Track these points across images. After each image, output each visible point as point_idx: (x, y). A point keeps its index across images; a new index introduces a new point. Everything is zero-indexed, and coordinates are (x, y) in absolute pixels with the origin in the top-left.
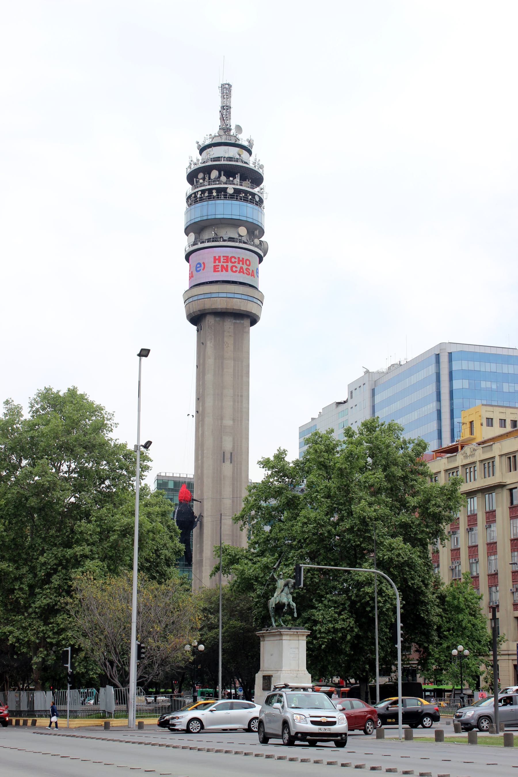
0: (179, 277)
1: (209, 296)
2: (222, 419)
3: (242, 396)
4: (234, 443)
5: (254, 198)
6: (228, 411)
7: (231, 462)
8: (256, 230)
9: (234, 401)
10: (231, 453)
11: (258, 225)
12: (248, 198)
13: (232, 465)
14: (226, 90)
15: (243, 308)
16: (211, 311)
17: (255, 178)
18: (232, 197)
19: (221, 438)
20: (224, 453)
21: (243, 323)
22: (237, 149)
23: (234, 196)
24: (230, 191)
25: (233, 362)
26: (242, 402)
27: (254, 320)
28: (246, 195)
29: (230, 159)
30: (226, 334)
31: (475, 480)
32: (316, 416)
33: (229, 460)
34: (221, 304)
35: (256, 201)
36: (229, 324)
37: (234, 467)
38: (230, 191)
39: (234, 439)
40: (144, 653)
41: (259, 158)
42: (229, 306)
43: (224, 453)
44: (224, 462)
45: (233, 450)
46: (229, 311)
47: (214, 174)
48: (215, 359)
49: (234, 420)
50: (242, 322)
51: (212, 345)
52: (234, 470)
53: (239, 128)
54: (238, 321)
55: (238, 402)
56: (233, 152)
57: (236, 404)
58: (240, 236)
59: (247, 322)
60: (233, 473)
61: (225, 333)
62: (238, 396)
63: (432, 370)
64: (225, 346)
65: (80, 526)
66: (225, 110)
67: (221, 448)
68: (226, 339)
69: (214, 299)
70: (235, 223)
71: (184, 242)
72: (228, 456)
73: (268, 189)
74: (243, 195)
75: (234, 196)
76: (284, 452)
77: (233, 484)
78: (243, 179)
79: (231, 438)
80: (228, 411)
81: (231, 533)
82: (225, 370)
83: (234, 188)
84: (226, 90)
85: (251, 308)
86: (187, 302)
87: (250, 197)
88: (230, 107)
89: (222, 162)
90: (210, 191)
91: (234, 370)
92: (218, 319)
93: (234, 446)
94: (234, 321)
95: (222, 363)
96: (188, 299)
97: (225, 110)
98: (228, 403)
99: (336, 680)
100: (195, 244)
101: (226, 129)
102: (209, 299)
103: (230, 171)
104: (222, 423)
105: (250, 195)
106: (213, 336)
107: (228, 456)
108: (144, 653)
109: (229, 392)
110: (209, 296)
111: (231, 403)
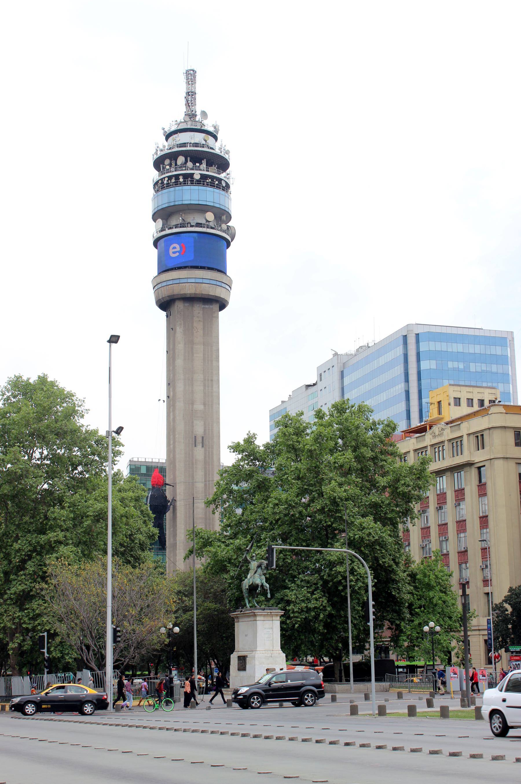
2: (193, 404)
3: (212, 380)
4: (205, 427)
5: (221, 183)
6: (199, 396)
7: (203, 446)
8: (223, 215)
9: (205, 386)
10: (203, 438)
11: (225, 210)
12: (214, 184)
13: (203, 449)
14: (191, 76)
15: (211, 293)
16: (179, 297)
17: (222, 164)
19: (193, 422)
20: (195, 437)
24: (197, 177)
26: (212, 386)
27: (222, 305)
29: (196, 145)
30: (195, 319)
31: (443, 459)
32: (286, 399)
33: (201, 445)
34: (189, 290)
35: (223, 187)
36: (198, 309)
37: (205, 450)
38: (197, 177)
39: (205, 424)
40: (119, 637)
43: (195, 437)
44: (195, 446)
45: (205, 434)
46: (198, 296)
47: (181, 160)
48: (185, 344)
49: (205, 404)
50: (211, 307)
52: (205, 454)
53: (204, 114)
54: (207, 306)
55: (208, 387)
56: (198, 138)
57: (207, 388)
58: (207, 221)
59: (216, 306)
60: (205, 457)
61: (194, 318)
62: (208, 380)
63: (399, 351)
66: (191, 96)
67: (193, 432)
68: (195, 324)
70: (202, 209)
72: (199, 440)
74: (210, 180)
77: (205, 468)
79: (202, 423)
80: (199, 396)
82: (195, 355)
84: (191, 76)
85: (219, 292)
87: (217, 182)
89: (189, 148)
90: (177, 177)
91: (204, 354)
92: (187, 305)
94: (203, 306)
95: (192, 348)
97: (191, 96)
98: (199, 388)
101: (191, 115)
102: (177, 285)
103: (195, 157)
104: (193, 408)
105: (216, 180)
106: (182, 322)
107: (199, 440)
108: (119, 637)
109: (199, 377)
111: (202, 388)
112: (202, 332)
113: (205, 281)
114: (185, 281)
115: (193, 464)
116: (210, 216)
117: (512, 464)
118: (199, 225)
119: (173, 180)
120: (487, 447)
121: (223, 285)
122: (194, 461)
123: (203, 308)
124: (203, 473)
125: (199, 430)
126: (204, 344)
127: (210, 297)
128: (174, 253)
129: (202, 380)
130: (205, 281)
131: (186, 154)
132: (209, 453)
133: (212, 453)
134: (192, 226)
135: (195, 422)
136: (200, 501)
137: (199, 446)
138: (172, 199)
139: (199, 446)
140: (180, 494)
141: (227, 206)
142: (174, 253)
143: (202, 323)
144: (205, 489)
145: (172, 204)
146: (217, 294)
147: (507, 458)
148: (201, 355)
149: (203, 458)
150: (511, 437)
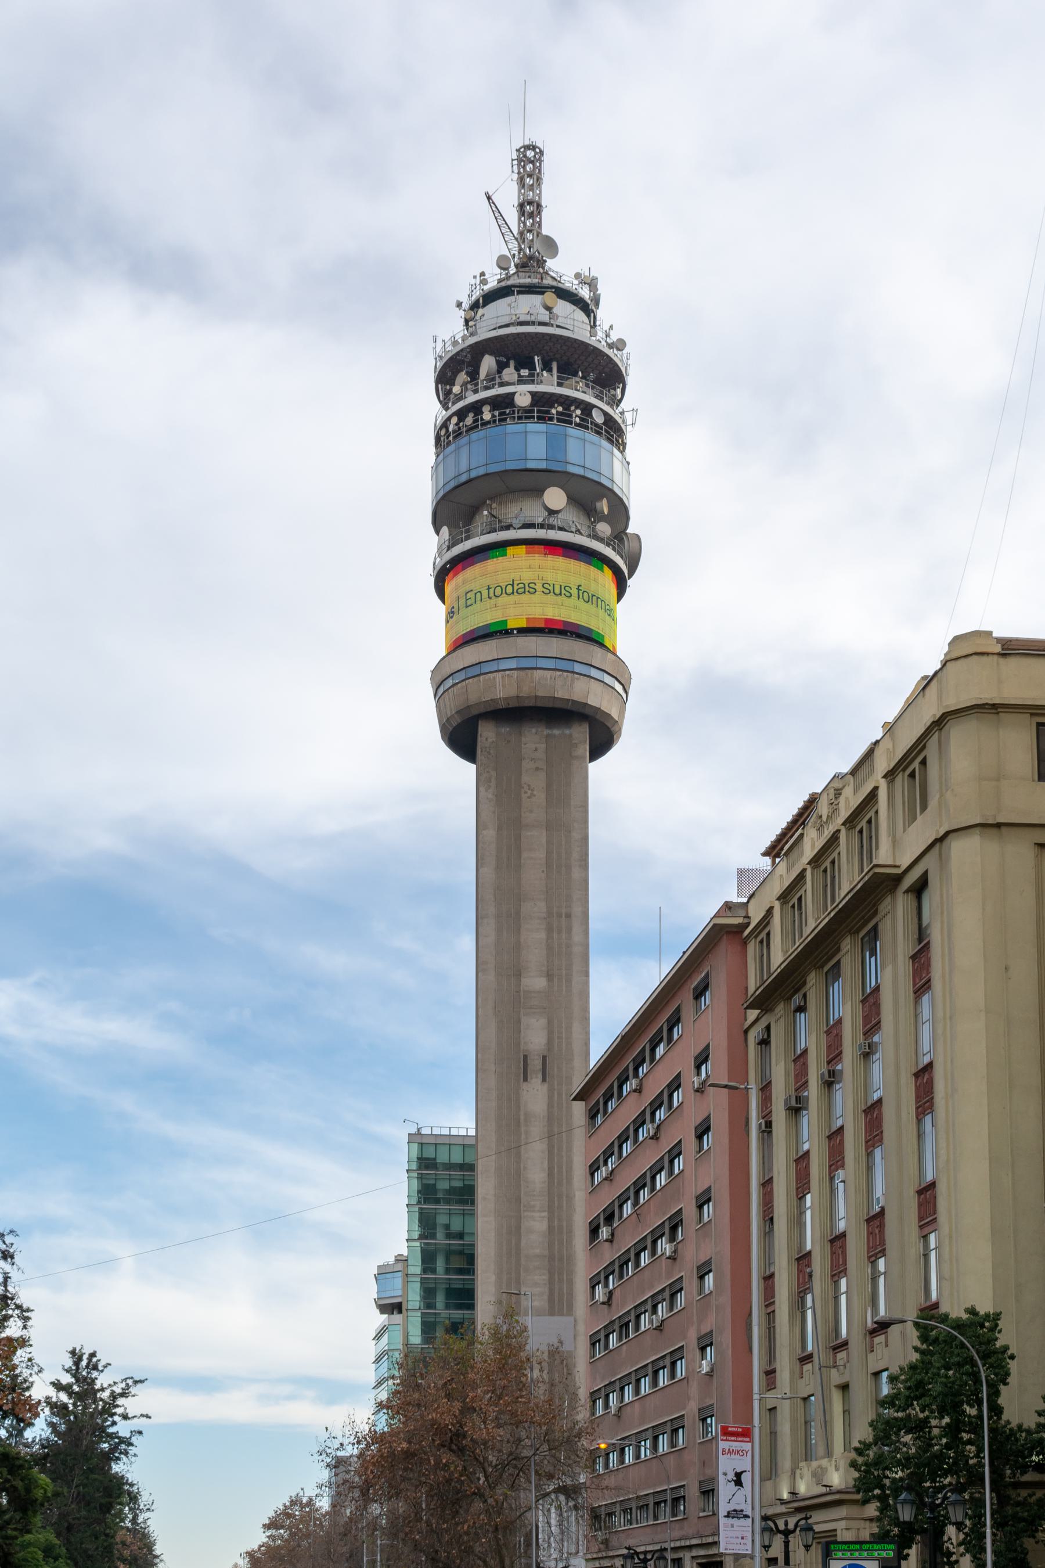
0: (425, 631)
1: (528, 666)
2: (518, 975)
3: (569, 916)
5: (590, 415)
6: (534, 955)
7: (544, 1080)
8: (601, 498)
9: (549, 930)
10: (544, 1058)
11: (600, 484)
12: (570, 416)
13: (546, 1086)
14: (529, 163)
15: (560, 694)
16: (483, 710)
17: (608, 376)
18: (526, 415)
19: (519, 1021)
20: (525, 1057)
21: (571, 735)
24: (523, 400)
25: (545, 834)
26: (569, 930)
28: (567, 408)
30: (526, 765)
33: (540, 1076)
35: (597, 425)
36: (533, 739)
37: (551, 1091)
38: (523, 400)
39: (550, 1022)
41: (616, 320)
43: (525, 1057)
44: (525, 1079)
45: (549, 1050)
47: (488, 363)
48: (500, 828)
49: (549, 976)
50: (567, 732)
51: (490, 796)
52: (550, 1098)
54: (556, 732)
55: (559, 932)
57: (555, 935)
58: (552, 513)
59: (580, 733)
60: (550, 1105)
61: (524, 763)
62: (560, 915)
64: (524, 796)
66: (530, 209)
68: (525, 778)
69: (486, 677)
71: (427, 547)
72: (536, 1064)
73: (637, 401)
74: (560, 409)
76: (264, 1526)
78: (567, 371)
79: (543, 1021)
80: (534, 955)
81: (546, 1253)
82: (525, 855)
84: (529, 163)
85: (595, 697)
86: (441, 691)
87: (578, 412)
88: (539, 206)
90: (476, 408)
91: (549, 853)
92: (505, 730)
94: (546, 732)
95: (518, 838)
96: (442, 681)
98: (534, 936)
100: (453, 543)
102: (475, 679)
103: (519, 351)
104: (518, 985)
106: (493, 773)
107: (536, 1064)
109: (535, 909)
110: (476, 671)
111: (543, 935)
112: (543, 796)
113: (542, 663)
114: (494, 666)
116: (555, 497)
117: (1020, 853)
119: (469, 420)
120: (933, 802)
121: (594, 673)
122: (522, 1118)
123: (547, 736)
125: (535, 1036)
126: (549, 827)
127: (558, 705)
129: (544, 915)
130: (542, 663)
135: (524, 1020)
136: (537, 1214)
137: (536, 1081)
138: (464, 467)
139: (536, 1081)
140: (484, 1199)
141: (604, 470)
143: (542, 775)
145: (464, 478)
146: (592, 701)
147: (999, 825)
148: (541, 854)
149: (546, 1108)
150: (1018, 746)
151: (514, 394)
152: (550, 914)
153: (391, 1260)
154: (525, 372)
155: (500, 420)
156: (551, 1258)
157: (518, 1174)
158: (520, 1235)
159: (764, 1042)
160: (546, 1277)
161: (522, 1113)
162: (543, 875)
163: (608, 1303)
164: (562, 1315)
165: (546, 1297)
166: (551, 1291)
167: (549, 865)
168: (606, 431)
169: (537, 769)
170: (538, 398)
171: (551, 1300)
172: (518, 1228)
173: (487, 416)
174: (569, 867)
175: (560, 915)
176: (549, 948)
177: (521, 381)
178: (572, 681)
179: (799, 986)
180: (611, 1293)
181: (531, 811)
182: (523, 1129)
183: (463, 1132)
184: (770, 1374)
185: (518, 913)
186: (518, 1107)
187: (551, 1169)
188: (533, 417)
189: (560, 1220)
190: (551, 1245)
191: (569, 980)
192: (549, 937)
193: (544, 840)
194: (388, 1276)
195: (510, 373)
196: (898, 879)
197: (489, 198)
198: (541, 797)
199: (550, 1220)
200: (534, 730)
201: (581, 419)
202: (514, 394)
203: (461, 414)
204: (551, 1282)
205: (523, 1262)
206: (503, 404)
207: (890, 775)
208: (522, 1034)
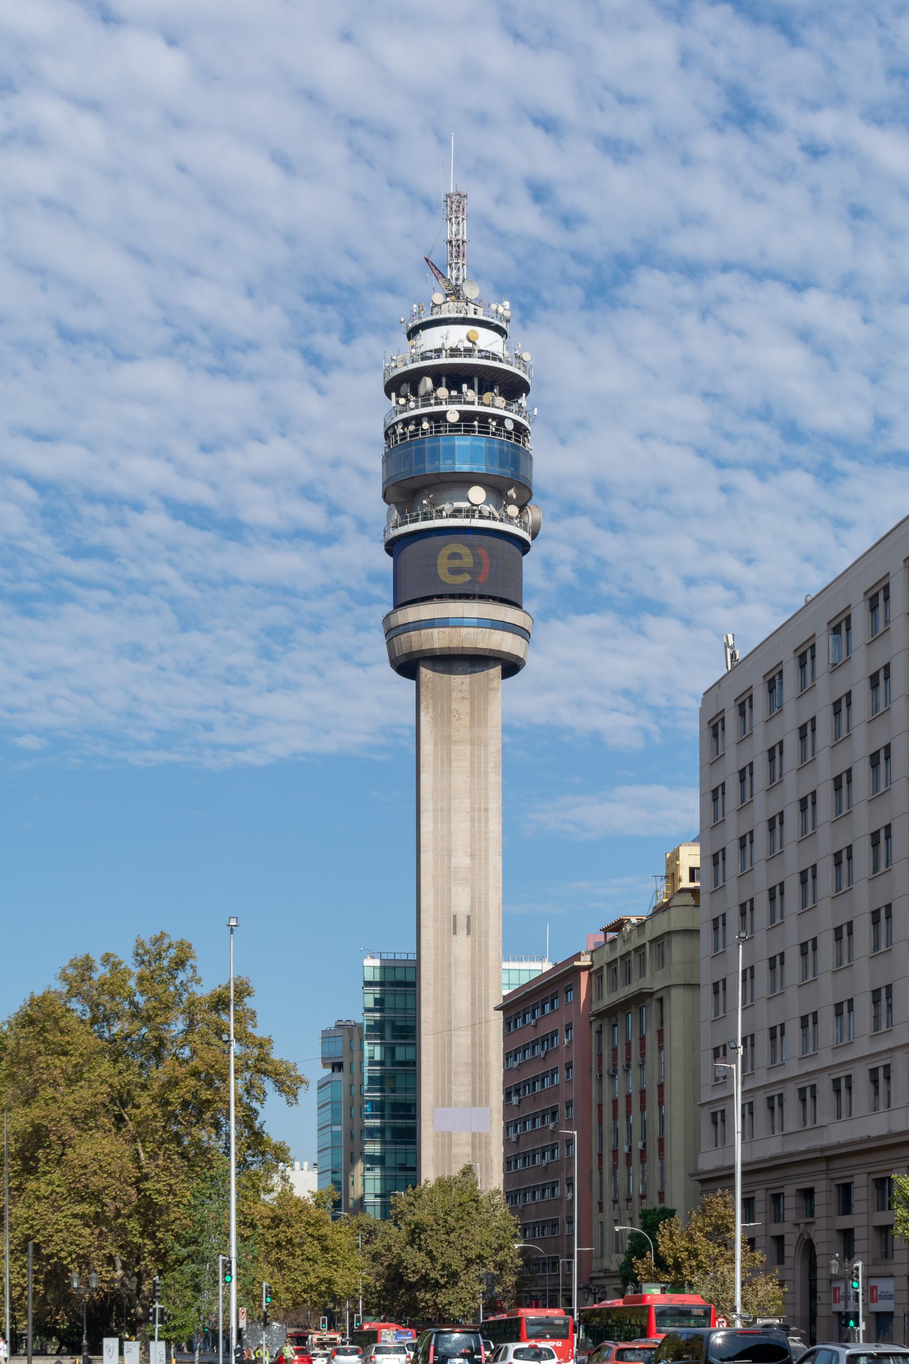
2: (450, 855)
3: (486, 810)
4: (473, 899)
7: (468, 933)
9: (472, 821)
10: (469, 917)
12: (488, 428)
13: (470, 937)
15: (481, 645)
19: (450, 890)
20: (455, 916)
22: (467, 329)
23: (460, 426)
24: (453, 417)
25: (469, 747)
29: (454, 352)
30: (455, 694)
37: (473, 941)
38: (453, 417)
39: (473, 890)
40: (159, 1291)
42: (455, 644)
43: (455, 916)
44: (455, 933)
45: (472, 911)
46: (455, 652)
48: (436, 744)
49: (472, 855)
51: (428, 719)
52: (473, 947)
55: (480, 822)
57: (477, 825)
61: (453, 694)
62: (480, 810)
64: (453, 718)
65: (140, 1096)
67: (450, 908)
68: (454, 705)
72: (462, 922)
75: (460, 426)
77: (473, 973)
81: (470, 1061)
82: (454, 764)
83: (459, 412)
87: (494, 423)
89: (444, 360)
91: (472, 762)
93: (473, 904)
95: (449, 752)
99: (852, 1323)
104: (450, 862)
105: (493, 420)
106: (431, 702)
107: (462, 922)
108: (159, 1291)
111: (468, 825)
115: (450, 966)
118: (456, 513)
122: (453, 961)
124: (469, 983)
126: (472, 743)
128: (454, 571)
131: (440, 375)
132: (480, 944)
133: (487, 945)
134: (481, 517)
135: (453, 888)
142: (454, 571)
144: (473, 1012)
148: (466, 763)
149: (469, 954)
151: (447, 411)
152: (473, 809)
153: (332, 1025)
154: (454, 393)
155: (436, 432)
156: (473, 1065)
157: (450, 1004)
158: (451, 1047)
159: (599, 1032)
160: (470, 1079)
161: (452, 958)
162: (468, 780)
163: (517, 1142)
164: (481, 1106)
165: (470, 1094)
166: (474, 1090)
167: (472, 772)
168: (515, 435)
169: (463, 698)
170: (466, 417)
171: (474, 1096)
172: (450, 1043)
173: (425, 425)
174: (486, 773)
175: (480, 810)
176: (473, 835)
177: (451, 400)
178: (490, 636)
179: (614, 1015)
180: (518, 1136)
181: (459, 731)
182: (453, 970)
183: (404, 957)
184: (601, 1204)
185: (449, 809)
186: (450, 954)
187: (473, 999)
188: (460, 431)
189: (480, 1037)
190: (473, 1056)
191: (486, 859)
192: (473, 826)
193: (468, 753)
194: (331, 1039)
195: (442, 392)
196: (652, 994)
197: (427, 260)
198: (466, 719)
199: (473, 1037)
200: (461, 668)
201: (497, 430)
202: (447, 411)
203: (406, 422)
204: (474, 1083)
205: (453, 1068)
206: (438, 418)
207: (651, 942)
208: (453, 899)
